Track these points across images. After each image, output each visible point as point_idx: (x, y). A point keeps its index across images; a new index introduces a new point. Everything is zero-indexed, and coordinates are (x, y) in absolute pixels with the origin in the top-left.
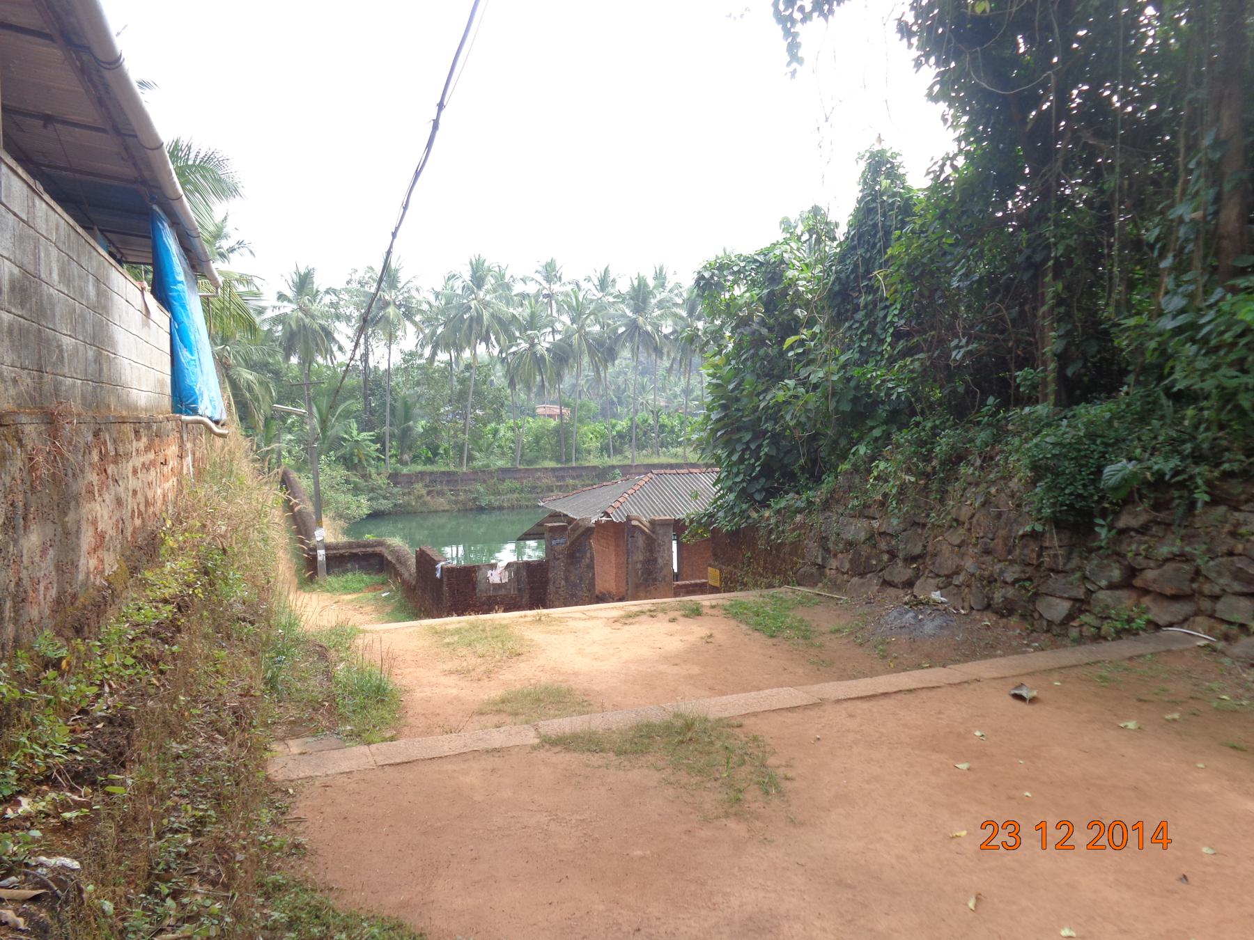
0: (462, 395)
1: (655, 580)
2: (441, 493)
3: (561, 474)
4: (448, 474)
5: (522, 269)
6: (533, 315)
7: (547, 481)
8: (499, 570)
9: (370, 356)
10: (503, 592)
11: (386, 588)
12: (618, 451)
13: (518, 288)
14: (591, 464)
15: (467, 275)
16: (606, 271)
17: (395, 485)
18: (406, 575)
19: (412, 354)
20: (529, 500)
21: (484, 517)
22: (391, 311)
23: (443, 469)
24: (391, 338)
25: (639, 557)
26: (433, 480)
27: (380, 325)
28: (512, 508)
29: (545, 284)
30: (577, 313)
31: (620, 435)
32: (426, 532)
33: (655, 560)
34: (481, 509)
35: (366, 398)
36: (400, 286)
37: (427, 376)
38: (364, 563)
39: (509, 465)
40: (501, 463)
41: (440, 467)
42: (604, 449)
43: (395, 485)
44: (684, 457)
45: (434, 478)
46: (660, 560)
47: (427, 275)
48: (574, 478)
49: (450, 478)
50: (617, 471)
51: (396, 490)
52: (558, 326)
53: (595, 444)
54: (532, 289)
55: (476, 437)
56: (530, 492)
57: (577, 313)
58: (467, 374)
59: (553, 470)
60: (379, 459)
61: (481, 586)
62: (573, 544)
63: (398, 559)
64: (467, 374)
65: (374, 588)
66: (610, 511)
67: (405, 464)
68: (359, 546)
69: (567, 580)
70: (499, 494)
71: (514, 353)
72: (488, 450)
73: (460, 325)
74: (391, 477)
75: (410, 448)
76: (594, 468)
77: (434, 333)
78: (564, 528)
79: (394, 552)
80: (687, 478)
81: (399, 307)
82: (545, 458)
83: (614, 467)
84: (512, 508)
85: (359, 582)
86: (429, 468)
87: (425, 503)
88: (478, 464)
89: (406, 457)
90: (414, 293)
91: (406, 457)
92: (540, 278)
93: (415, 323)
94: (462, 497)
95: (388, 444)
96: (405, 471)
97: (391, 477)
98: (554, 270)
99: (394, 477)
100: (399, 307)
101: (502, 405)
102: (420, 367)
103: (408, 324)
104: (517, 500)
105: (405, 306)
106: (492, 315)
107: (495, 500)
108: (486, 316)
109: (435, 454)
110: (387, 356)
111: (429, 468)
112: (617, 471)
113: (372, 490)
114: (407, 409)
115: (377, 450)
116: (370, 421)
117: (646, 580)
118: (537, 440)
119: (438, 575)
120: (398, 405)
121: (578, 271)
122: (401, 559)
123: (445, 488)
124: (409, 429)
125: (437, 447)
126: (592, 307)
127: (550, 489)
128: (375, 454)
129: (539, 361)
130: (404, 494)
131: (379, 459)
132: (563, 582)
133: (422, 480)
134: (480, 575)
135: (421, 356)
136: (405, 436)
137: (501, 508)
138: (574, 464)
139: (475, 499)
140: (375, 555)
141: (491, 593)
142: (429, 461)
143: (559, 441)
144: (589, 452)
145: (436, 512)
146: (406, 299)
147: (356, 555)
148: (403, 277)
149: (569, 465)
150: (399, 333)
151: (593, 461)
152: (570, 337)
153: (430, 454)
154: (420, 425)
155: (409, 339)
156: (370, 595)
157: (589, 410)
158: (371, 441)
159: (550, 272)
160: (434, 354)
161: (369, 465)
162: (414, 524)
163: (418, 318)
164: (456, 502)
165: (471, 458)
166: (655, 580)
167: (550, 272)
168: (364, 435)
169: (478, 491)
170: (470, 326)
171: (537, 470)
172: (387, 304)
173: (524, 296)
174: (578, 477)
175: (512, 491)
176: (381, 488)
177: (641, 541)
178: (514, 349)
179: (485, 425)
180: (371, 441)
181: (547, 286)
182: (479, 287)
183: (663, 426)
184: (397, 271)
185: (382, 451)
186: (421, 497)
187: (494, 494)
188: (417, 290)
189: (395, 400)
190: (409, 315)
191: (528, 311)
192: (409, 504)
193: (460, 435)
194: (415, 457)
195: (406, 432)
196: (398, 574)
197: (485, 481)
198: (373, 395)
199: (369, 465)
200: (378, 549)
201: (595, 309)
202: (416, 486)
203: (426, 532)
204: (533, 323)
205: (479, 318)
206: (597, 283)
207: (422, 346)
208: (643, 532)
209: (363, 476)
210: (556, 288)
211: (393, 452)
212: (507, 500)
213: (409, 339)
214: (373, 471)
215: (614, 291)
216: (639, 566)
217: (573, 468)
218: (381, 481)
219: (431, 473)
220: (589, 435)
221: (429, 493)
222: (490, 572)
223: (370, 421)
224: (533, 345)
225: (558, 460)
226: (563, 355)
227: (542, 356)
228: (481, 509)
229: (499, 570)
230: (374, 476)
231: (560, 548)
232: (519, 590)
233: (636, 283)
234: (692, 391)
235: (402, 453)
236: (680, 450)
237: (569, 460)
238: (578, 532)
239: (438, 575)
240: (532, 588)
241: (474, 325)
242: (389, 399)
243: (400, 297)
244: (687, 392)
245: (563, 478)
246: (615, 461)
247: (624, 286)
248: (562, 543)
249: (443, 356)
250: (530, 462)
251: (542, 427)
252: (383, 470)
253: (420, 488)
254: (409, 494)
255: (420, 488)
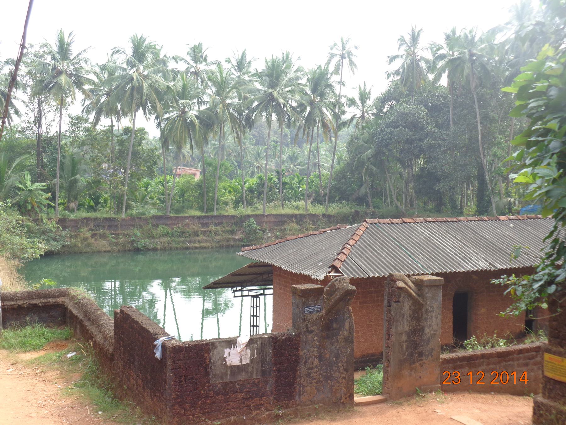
0: (122, 154)
1: (421, 354)
2: (104, 237)
3: (206, 221)
4: (110, 220)
5: (174, 47)
6: (184, 87)
7: (194, 227)
8: (239, 349)
9: (43, 119)
10: (242, 376)
11: (71, 346)
12: (250, 203)
13: (171, 65)
14: (230, 214)
15: (129, 52)
16: (244, 55)
17: (64, 228)
18: (99, 338)
19: (78, 119)
20: (179, 243)
21: (140, 257)
22: (63, 79)
23: (105, 216)
24: (62, 103)
25: (404, 326)
26: (97, 225)
27: (53, 91)
28: (164, 249)
29: (192, 63)
30: (222, 87)
31: (251, 190)
32: (90, 269)
33: (423, 329)
34: (138, 250)
35: (39, 154)
36: (71, 57)
37: (92, 138)
38: (44, 315)
39: (160, 214)
40: (153, 212)
41: (101, 214)
42: (237, 203)
43: (64, 228)
44: (306, 209)
45: (97, 223)
46: (427, 331)
47: (99, 49)
48: (216, 225)
49: (111, 223)
50: (252, 220)
51: (64, 233)
52: (206, 98)
53: (230, 198)
54: (181, 67)
55: (133, 189)
56: (179, 236)
57: (222, 87)
58: (125, 137)
59: (199, 218)
60: (49, 206)
61: (217, 370)
62: (329, 312)
63: (86, 314)
64: (125, 137)
65: (57, 345)
66: (338, 264)
67: (72, 211)
68: (38, 295)
69: (320, 357)
70: (153, 238)
71: (167, 119)
72: (143, 200)
73: (123, 94)
74: (60, 221)
75: (76, 198)
76: (233, 217)
77: (98, 101)
78: (319, 292)
79: (80, 305)
80: (403, 228)
81: (70, 76)
82: (192, 208)
83: (249, 216)
84: (164, 249)
85: (40, 336)
86: (92, 215)
87: (89, 245)
88: (134, 212)
89: (73, 205)
90: (83, 64)
91: (73, 205)
92: (188, 58)
93: (84, 92)
94: (121, 240)
95: (58, 194)
96: (72, 216)
97: (60, 221)
98: (200, 52)
99: (63, 222)
100: (70, 76)
101: (155, 163)
102: (86, 130)
103: (77, 91)
104: (169, 243)
105: (75, 75)
106: (151, 86)
107: (150, 243)
108: (146, 85)
109: (97, 203)
110: (57, 120)
111: (92, 215)
112: (252, 220)
113: (44, 233)
114: (74, 164)
115: (47, 199)
116: (41, 174)
117: (411, 355)
118: (182, 193)
119: (158, 355)
120: (67, 161)
121: (221, 54)
122: (91, 316)
123: (107, 232)
124: (76, 181)
125: (98, 198)
126: (233, 83)
127: (196, 234)
128: (46, 202)
129: (189, 126)
130: (71, 237)
131: (49, 206)
132: (316, 362)
133: (87, 224)
134: (215, 355)
135: (86, 120)
136: (71, 189)
137: (155, 250)
138: (215, 213)
139: (133, 242)
140: (56, 306)
141: (228, 379)
142: (91, 208)
143: (201, 194)
144: (226, 203)
145: (99, 252)
146: (77, 70)
147: (36, 306)
148: (74, 50)
149: (211, 214)
150: (69, 100)
151: (231, 211)
152: (216, 106)
153: (92, 203)
154: (83, 180)
155: (77, 105)
156: (53, 354)
157: (226, 169)
158: (42, 190)
159: (197, 54)
160: (97, 120)
161: (42, 211)
162: (80, 263)
163: (87, 87)
164: (117, 244)
165: (129, 207)
166: (421, 354)
167: (197, 54)
168: (37, 185)
169: (135, 235)
170: (132, 94)
171: (185, 218)
172: (60, 73)
173: (176, 72)
174: (220, 224)
175: (165, 235)
176: (51, 231)
177: (407, 307)
178: (167, 116)
179: (139, 179)
180: (42, 190)
181: (195, 65)
182: (140, 61)
183: (285, 184)
184: (69, 44)
185: (53, 199)
186: (85, 239)
187: (149, 238)
188: (86, 62)
189: (64, 157)
190: (79, 83)
191: (180, 84)
192: (76, 245)
193: (120, 186)
194: (80, 205)
195: (73, 183)
196: (87, 336)
197: (141, 227)
198: (45, 152)
199: (42, 211)
200: (60, 300)
201: (235, 85)
202: (81, 230)
203: (90, 269)
204: (184, 94)
205: (140, 89)
206: (235, 64)
207: (88, 112)
208: (410, 295)
209: (36, 221)
210: (202, 67)
211: (61, 201)
212: (159, 242)
213: (77, 105)
214: (44, 216)
215: (252, 70)
216: (404, 338)
217: (215, 217)
218: (52, 225)
219: (95, 219)
220: (225, 190)
221: (93, 236)
222: (227, 351)
223: (41, 174)
224: (184, 113)
225: (201, 209)
226: (209, 122)
227: (192, 123)
228: (138, 250)
229: (239, 349)
230: (45, 220)
231: (315, 316)
232: (263, 373)
233: (270, 64)
234: (297, 158)
235: (69, 202)
236: (301, 203)
237: (212, 210)
238: (335, 297)
239: (158, 355)
240: (278, 370)
241: (135, 93)
242: (59, 157)
243: (72, 67)
244: (293, 158)
245: (207, 225)
246: (249, 211)
247: (259, 66)
248: (315, 311)
249: (105, 122)
250: (177, 211)
251: (188, 182)
252: (53, 216)
253: (85, 232)
254: (76, 236)
255: (85, 232)
